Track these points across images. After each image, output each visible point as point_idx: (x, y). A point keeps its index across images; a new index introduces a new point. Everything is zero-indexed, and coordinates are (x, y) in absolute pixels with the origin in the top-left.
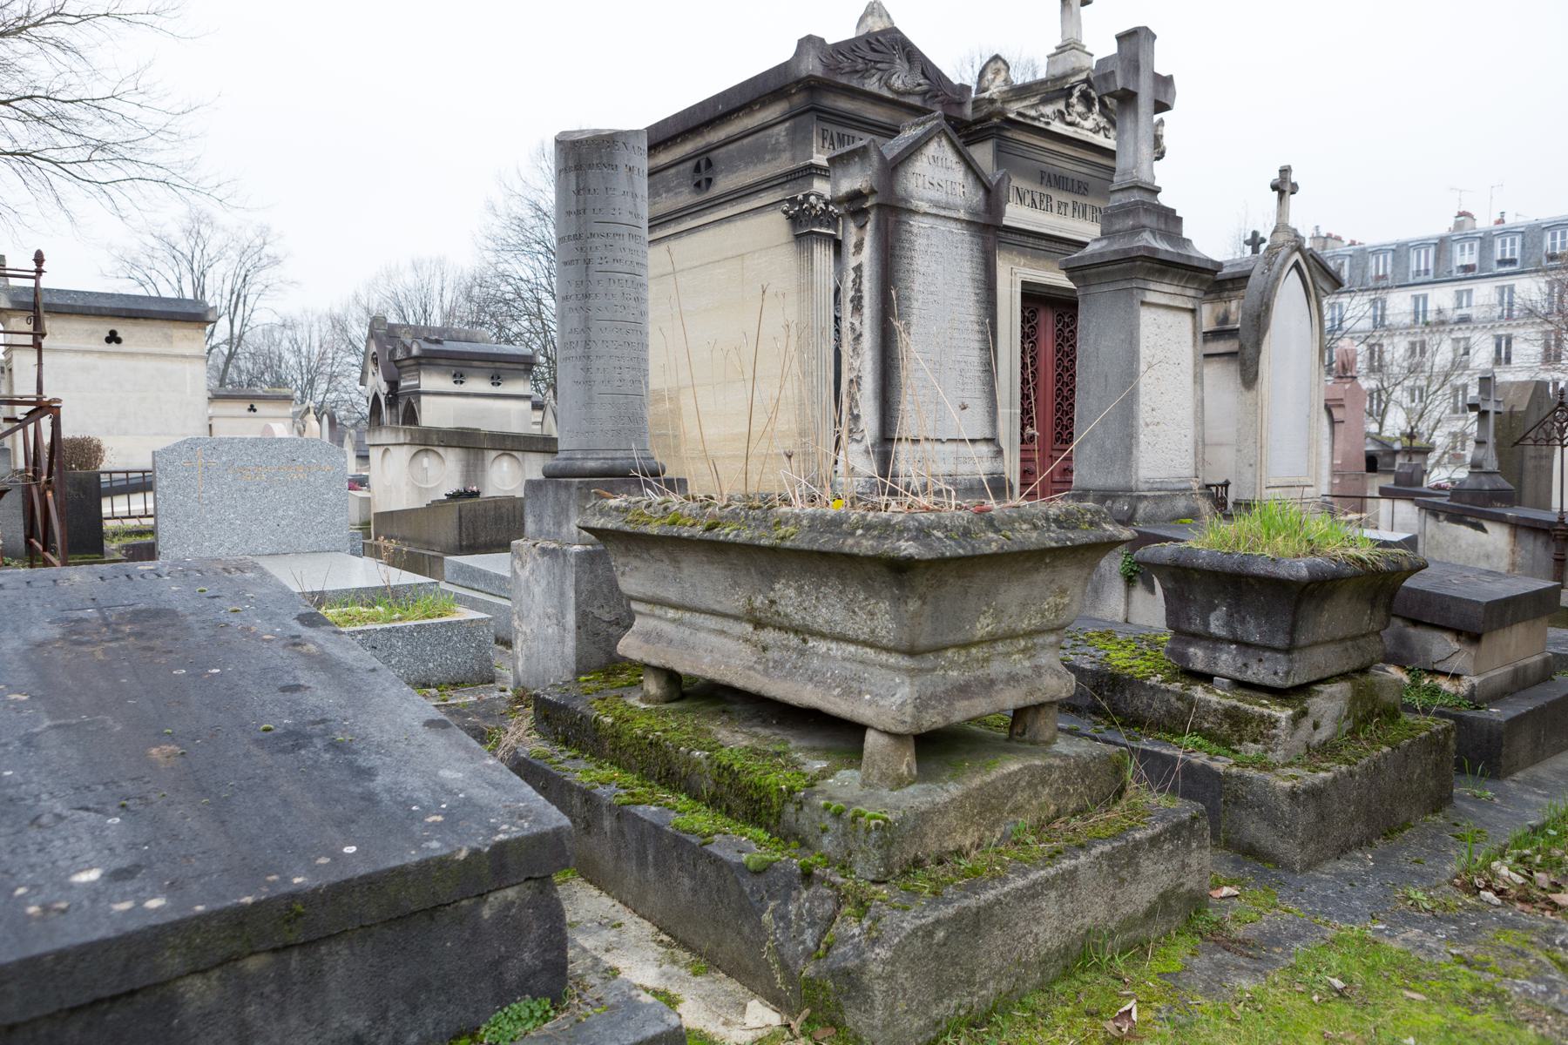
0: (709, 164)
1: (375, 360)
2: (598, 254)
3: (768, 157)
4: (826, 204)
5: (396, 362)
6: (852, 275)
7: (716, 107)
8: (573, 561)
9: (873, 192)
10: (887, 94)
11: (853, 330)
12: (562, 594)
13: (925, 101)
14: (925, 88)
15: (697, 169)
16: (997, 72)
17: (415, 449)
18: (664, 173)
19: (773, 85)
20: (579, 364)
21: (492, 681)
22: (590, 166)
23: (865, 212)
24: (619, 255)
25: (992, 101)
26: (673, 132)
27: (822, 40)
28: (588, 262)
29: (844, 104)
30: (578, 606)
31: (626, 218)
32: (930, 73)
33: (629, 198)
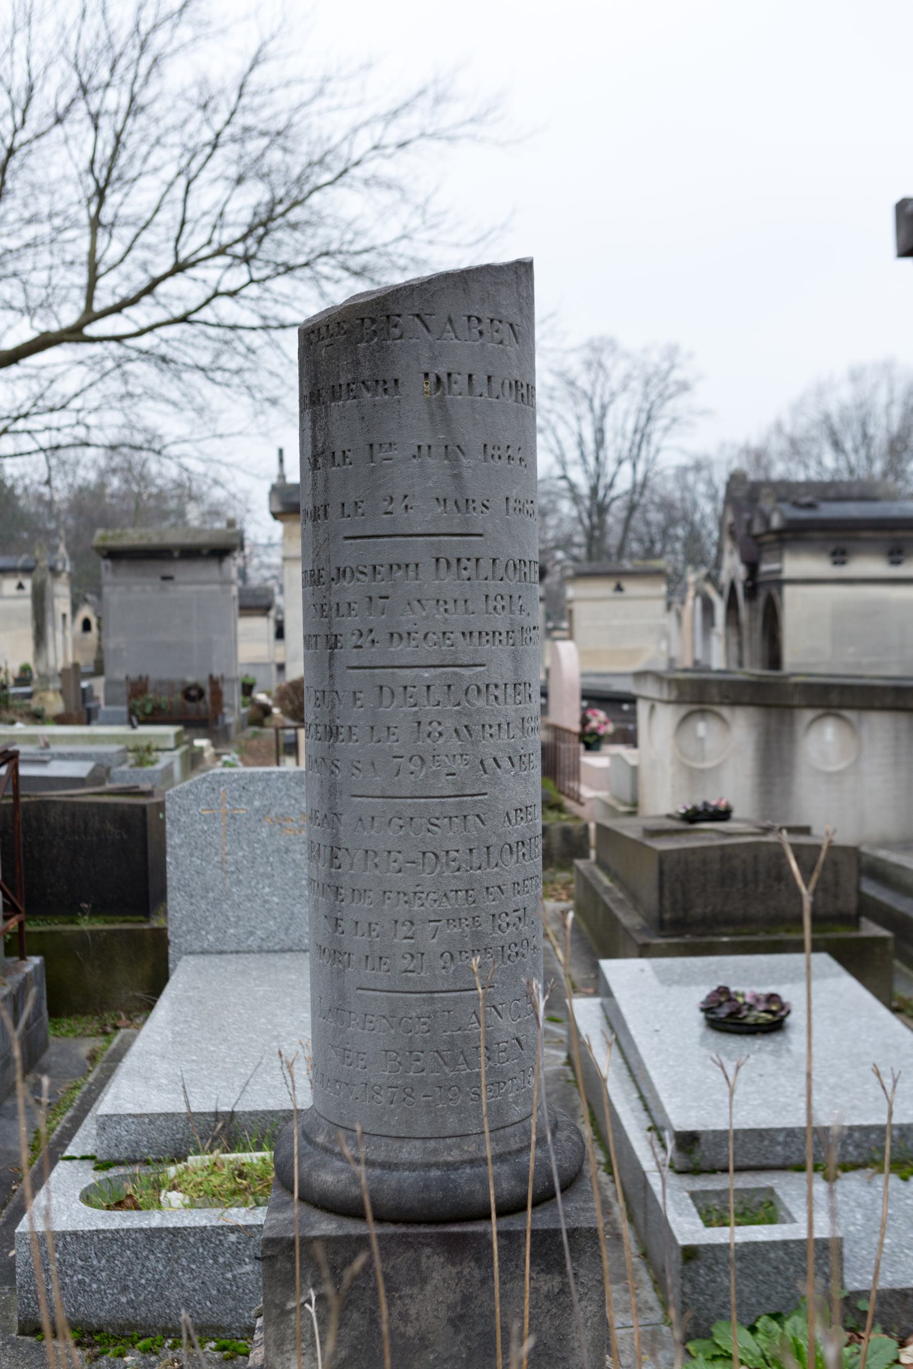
1: (733, 534)
5: (756, 537)
17: (684, 710)
31: (423, 517)
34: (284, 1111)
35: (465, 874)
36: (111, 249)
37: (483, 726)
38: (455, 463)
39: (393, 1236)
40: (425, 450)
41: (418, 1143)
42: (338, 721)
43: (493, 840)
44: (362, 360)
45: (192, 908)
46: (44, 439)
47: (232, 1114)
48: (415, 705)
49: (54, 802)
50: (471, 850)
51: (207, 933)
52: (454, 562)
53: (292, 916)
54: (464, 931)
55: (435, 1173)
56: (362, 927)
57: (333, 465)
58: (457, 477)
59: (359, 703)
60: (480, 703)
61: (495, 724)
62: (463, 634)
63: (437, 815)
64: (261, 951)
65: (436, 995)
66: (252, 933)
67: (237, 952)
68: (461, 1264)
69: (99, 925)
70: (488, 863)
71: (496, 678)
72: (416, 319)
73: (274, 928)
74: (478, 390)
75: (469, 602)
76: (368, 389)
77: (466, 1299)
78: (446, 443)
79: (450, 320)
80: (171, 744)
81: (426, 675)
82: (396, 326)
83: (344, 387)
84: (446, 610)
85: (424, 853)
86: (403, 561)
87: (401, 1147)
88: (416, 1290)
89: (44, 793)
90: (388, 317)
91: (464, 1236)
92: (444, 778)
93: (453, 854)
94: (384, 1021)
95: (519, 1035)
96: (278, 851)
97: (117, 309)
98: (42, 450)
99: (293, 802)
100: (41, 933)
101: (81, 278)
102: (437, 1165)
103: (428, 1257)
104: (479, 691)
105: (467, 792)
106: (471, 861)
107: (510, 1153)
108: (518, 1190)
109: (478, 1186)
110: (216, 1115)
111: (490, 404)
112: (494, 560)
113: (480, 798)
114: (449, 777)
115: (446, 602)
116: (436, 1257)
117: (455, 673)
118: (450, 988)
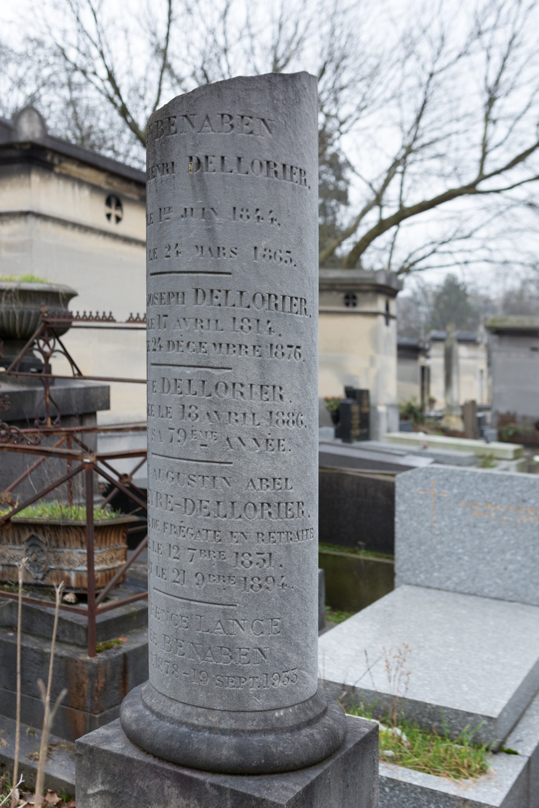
34: (387, 695)
35: (214, 519)
36: (497, 133)
37: (230, 413)
38: (209, 221)
39: (148, 765)
40: (189, 211)
41: (181, 706)
43: (238, 498)
45: (411, 554)
46: (460, 257)
47: (353, 688)
48: (181, 393)
49: (348, 475)
50: (218, 502)
51: (420, 573)
52: (208, 292)
53: (477, 572)
54: (212, 561)
55: (184, 729)
58: (211, 230)
60: (228, 396)
61: (240, 412)
62: (214, 344)
63: (194, 473)
64: (455, 591)
65: (192, 603)
66: (449, 578)
67: (439, 589)
68: (189, 799)
69: (371, 558)
70: (233, 514)
71: (240, 378)
72: (185, 119)
73: (465, 578)
74: (229, 168)
75: (219, 322)
78: (203, 206)
79: (207, 117)
80: (510, 456)
81: (188, 372)
82: (173, 125)
84: (202, 327)
85: (186, 500)
86: (175, 290)
87: (171, 705)
89: (343, 468)
90: (169, 119)
91: (191, 779)
92: (199, 447)
93: (205, 503)
94: (164, 614)
95: (262, 646)
96: (468, 525)
97: (498, 172)
98: (458, 263)
99: (480, 493)
100: (334, 556)
101: (478, 154)
102: (186, 724)
103: (169, 787)
104: (226, 387)
105: (216, 460)
106: (218, 510)
107: (243, 731)
108: (235, 758)
109: (204, 747)
110: (344, 686)
111: (240, 178)
112: (241, 293)
113: (226, 465)
114: (202, 447)
115: (202, 321)
116: (173, 789)
117: (208, 373)
118: (201, 599)
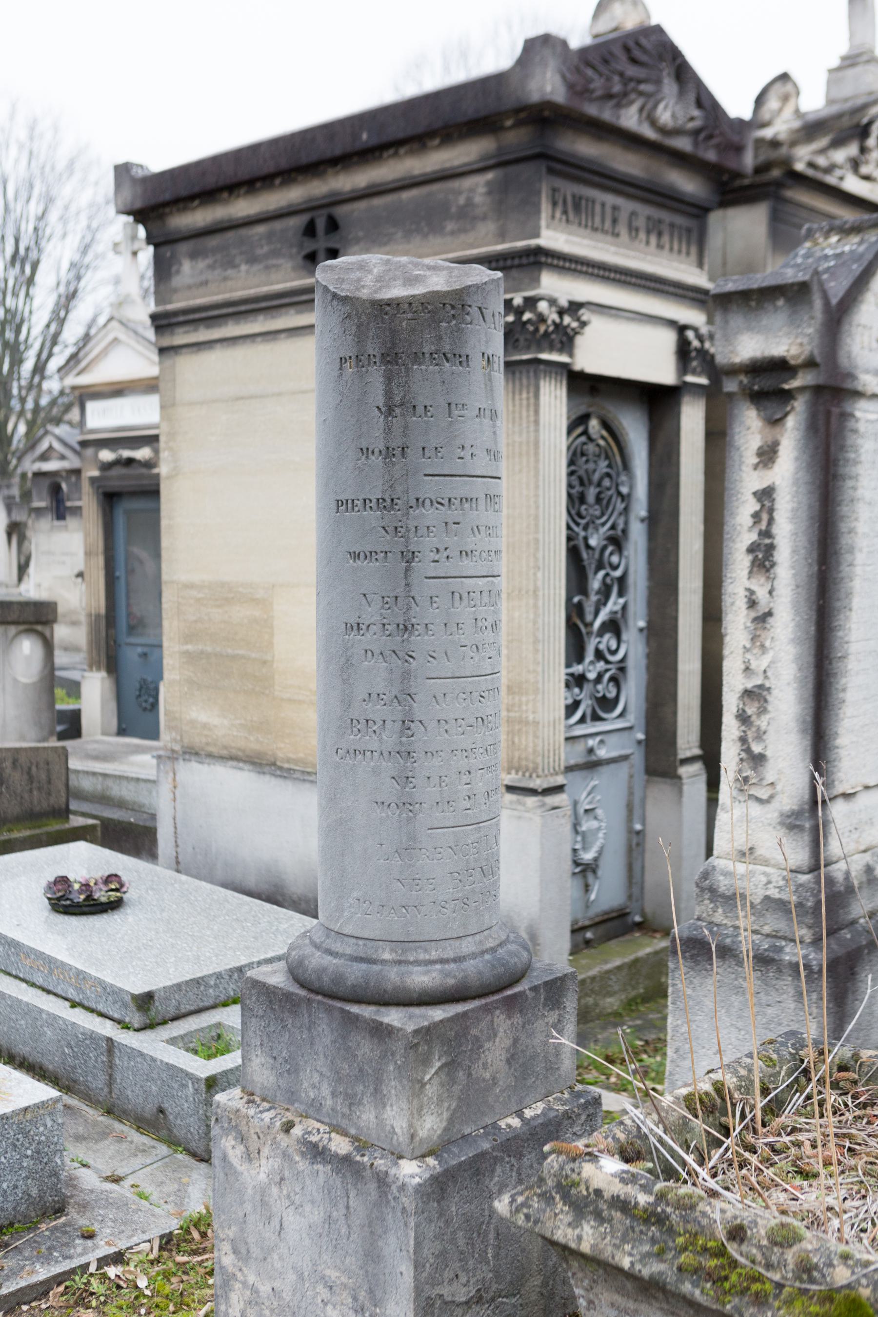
0: (333, 225)
2: (430, 541)
3: (450, 226)
4: (561, 313)
6: (752, 506)
7: (356, 136)
8: (408, 1202)
9: (810, 364)
10: (649, 133)
11: (752, 604)
12: (372, 1256)
13: (696, 144)
14: (697, 124)
15: (310, 230)
16: (785, 98)
18: (244, 232)
19: (470, 109)
20: (388, 767)
21: (59, 1210)
22: (417, 358)
23: (787, 396)
24: (471, 542)
25: (775, 144)
26: (269, 167)
27: (564, 43)
28: (409, 557)
29: (586, 148)
30: (418, 1290)
31: (481, 465)
32: (706, 103)
33: (487, 421)
42: (414, 621)
44: (444, 336)
56: (435, 780)
57: (414, 415)
59: (435, 605)
76: (447, 360)
77: (516, 1041)
83: (427, 356)
86: (469, 497)
88: (491, 1043)
